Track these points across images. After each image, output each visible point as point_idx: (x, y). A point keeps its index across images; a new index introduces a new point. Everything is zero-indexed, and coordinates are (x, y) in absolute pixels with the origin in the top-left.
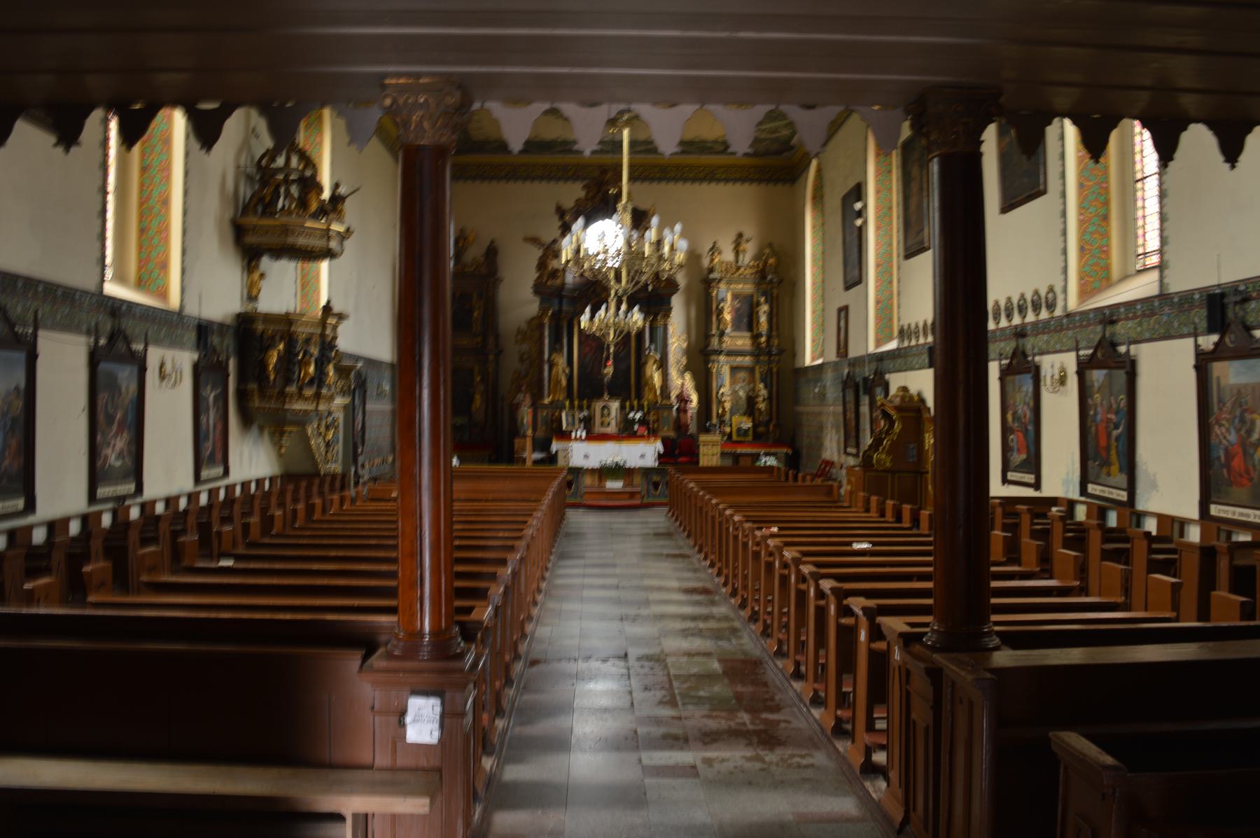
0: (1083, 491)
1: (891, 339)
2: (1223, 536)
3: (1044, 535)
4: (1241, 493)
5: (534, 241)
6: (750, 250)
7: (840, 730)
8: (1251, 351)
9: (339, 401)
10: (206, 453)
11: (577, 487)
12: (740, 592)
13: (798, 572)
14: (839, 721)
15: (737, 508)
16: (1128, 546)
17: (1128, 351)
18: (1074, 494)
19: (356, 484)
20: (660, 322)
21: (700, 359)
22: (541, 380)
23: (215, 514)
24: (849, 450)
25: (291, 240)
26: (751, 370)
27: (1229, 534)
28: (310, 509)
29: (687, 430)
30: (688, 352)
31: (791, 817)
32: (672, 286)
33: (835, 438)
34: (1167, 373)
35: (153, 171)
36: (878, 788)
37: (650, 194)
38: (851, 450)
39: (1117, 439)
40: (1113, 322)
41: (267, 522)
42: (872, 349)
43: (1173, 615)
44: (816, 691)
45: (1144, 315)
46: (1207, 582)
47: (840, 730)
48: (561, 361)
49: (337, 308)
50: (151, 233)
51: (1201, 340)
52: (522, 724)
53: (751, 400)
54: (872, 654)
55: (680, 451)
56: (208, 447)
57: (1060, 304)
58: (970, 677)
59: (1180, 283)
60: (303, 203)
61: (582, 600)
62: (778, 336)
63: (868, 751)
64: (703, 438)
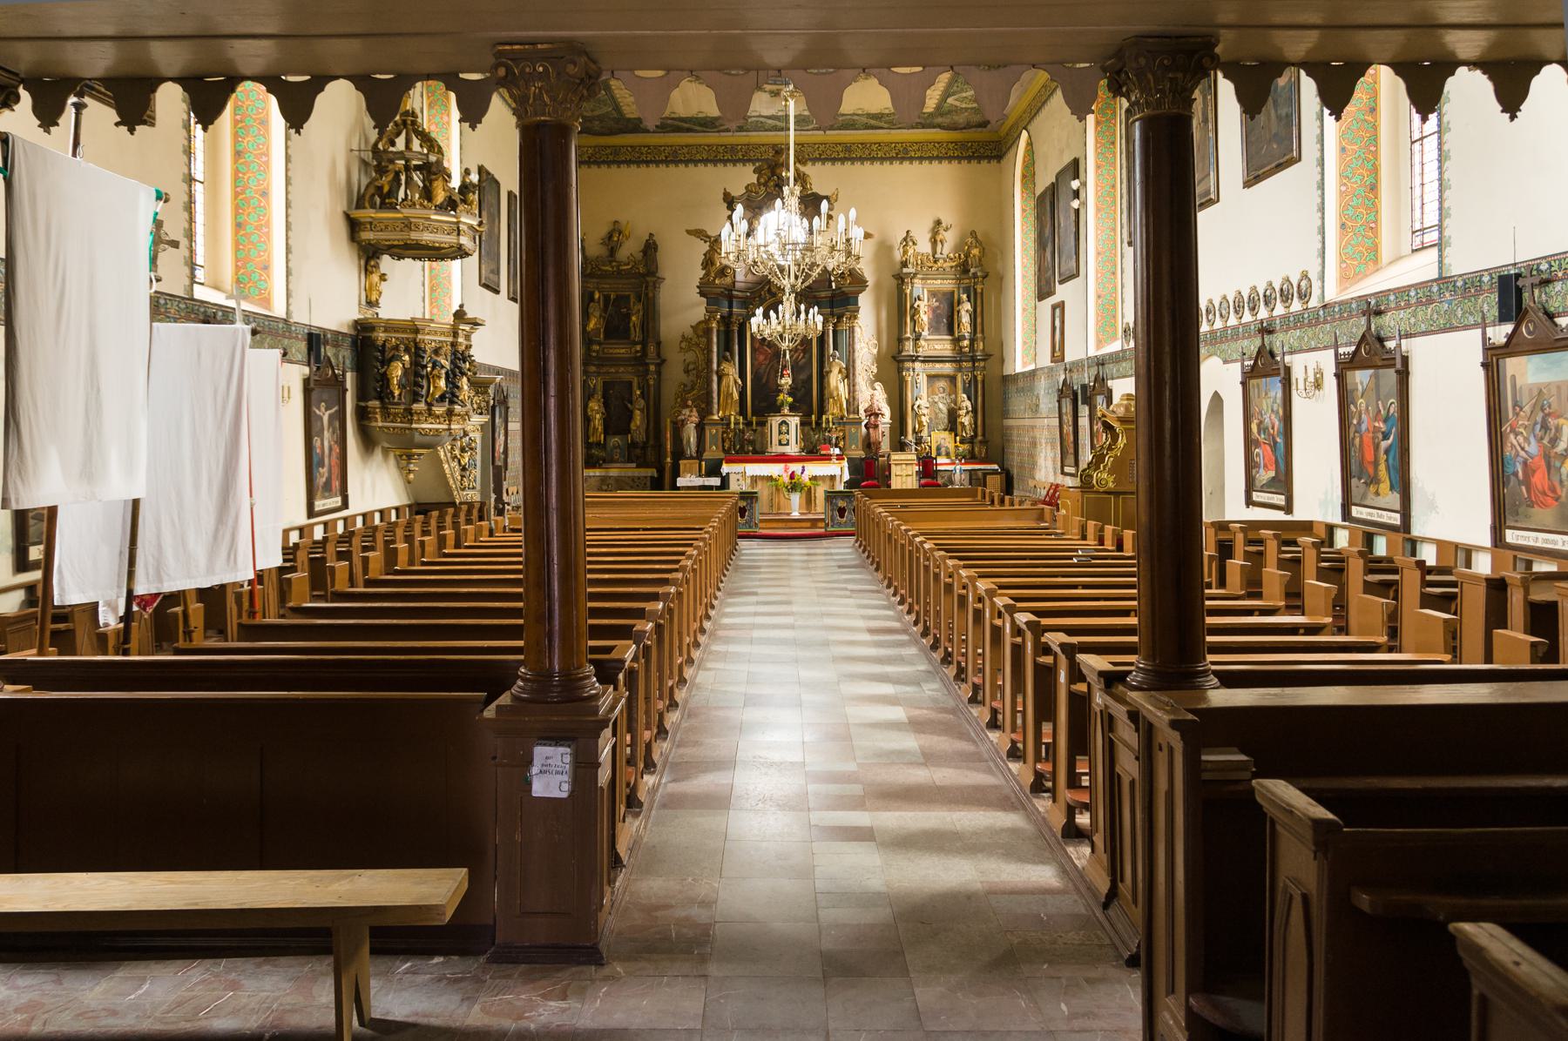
0: (1346, 514)
1: (1114, 339)
2: (1521, 566)
3: (1294, 565)
4: (1545, 515)
5: (700, 234)
6: (949, 239)
7: (1038, 787)
8: (1557, 343)
9: (477, 420)
10: (321, 481)
11: (752, 517)
12: (933, 631)
13: (993, 604)
14: (1039, 776)
15: (929, 535)
16: (1396, 577)
17: (1399, 345)
18: (1335, 517)
19: (500, 512)
20: (844, 326)
21: (893, 367)
22: (709, 393)
23: (331, 549)
24: (1067, 469)
25: (414, 236)
26: (952, 379)
27: (1529, 564)
28: (442, 541)
29: (878, 448)
30: (879, 359)
31: (979, 886)
32: (859, 282)
33: (1050, 454)
34: (1447, 374)
35: (249, 157)
36: (1080, 854)
37: (822, 177)
38: (1072, 470)
39: (1387, 452)
40: (1379, 313)
41: (391, 556)
42: (1092, 352)
43: (1448, 657)
44: (1014, 743)
45: (1419, 303)
46: (1497, 615)
47: (1038, 787)
48: (732, 371)
49: (471, 314)
50: (249, 229)
51: (1490, 331)
52: (674, 781)
53: (953, 415)
54: (1072, 696)
55: (870, 473)
56: (322, 474)
57: (1316, 292)
58: (1166, 718)
59: (1462, 263)
60: (428, 194)
61: (751, 641)
62: (983, 339)
63: (1071, 811)
64: (895, 457)
